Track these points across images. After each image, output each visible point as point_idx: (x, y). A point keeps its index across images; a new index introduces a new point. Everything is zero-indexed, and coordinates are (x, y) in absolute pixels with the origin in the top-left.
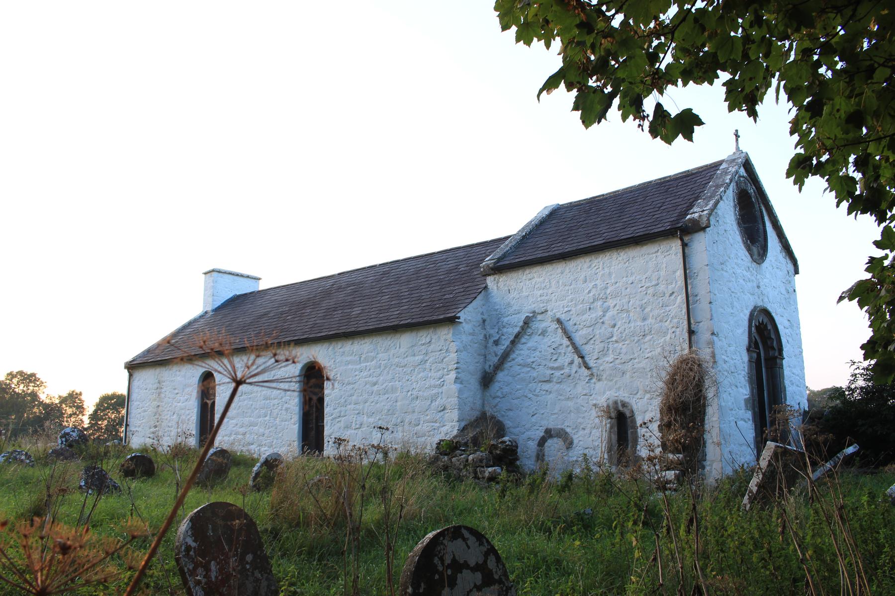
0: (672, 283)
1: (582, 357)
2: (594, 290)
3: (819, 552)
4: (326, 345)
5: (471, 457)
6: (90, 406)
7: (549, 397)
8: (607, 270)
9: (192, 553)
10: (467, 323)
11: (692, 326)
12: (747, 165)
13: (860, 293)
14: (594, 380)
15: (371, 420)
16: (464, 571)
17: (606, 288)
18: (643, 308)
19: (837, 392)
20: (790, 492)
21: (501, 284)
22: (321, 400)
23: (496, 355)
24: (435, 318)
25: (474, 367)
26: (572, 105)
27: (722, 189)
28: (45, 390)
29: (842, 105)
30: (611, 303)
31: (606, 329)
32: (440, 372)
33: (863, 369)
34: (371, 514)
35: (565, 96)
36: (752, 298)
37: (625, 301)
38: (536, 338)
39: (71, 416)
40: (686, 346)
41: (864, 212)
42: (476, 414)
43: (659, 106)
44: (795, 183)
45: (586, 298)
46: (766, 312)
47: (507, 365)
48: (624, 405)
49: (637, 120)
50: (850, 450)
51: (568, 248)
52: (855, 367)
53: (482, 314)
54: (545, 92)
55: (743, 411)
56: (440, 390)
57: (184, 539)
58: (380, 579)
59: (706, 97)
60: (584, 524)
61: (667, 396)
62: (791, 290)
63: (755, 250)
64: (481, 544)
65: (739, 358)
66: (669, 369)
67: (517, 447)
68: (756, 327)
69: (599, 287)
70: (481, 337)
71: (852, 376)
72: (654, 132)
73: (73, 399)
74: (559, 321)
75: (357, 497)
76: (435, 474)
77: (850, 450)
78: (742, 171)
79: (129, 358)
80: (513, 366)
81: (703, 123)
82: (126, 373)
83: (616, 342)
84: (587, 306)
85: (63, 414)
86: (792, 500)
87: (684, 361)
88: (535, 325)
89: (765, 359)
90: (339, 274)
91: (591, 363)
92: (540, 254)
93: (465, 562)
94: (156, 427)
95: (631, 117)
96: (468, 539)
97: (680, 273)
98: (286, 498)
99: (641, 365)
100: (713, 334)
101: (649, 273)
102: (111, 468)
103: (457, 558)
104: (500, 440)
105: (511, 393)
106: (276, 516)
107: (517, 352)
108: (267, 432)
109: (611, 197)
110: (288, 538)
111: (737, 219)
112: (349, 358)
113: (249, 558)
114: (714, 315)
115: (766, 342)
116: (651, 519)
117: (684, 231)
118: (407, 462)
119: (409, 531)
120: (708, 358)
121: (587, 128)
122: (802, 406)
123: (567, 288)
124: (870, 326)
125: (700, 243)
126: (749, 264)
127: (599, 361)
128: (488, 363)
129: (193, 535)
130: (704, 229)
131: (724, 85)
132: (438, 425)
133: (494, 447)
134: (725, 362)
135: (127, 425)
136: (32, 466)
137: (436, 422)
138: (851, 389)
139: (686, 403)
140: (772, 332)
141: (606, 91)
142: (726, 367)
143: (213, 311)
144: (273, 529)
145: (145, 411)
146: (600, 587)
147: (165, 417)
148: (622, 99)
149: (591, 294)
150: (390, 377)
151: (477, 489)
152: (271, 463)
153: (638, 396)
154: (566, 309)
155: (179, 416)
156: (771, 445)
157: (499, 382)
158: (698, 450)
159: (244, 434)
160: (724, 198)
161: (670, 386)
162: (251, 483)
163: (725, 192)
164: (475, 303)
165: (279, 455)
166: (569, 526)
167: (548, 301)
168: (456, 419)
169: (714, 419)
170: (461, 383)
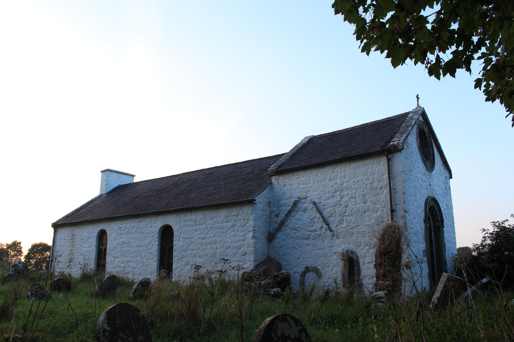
1: (328, 225)
2: (335, 185)
4: (175, 215)
5: (263, 282)
6: (25, 251)
7: (308, 247)
9: (107, 334)
10: (260, 203)
11: (393, 207)
12: (424, 115)
14: (335, 238)
17: (343, 184)
18: (364, 196)
21: (280, 181)
22: (171, 248)
23: (277, 223)
24: (241, 200)
27: (410, 128)
30: (345, 193)
31: (342, 208)
32: (244, 232)
36: (426, 191)
37: (353, 192)
38: (301, 213)
39: (13, 256)
45: (331, 190)
46: (434, 200)
48: (353, 252)
50: (484, 280)
51: (320, 161)
52: (485, 232)
53: (269, 198)
56: (243, 243)
57: (102, 325)
61: (379, 247)
62: (448, 188)
63: (428, 164)
64: (297, 325)
65: (420, 226)
67: (290, 276)
70: (268, 212)
71: (483, 238)
72: (431, 73)
73: (16, 246)
74: (314, 203)
77: (484, 280)
78: (421, 118)
79: (55, 220)
82: (52, 230)
83: (348, 216)
87: (389, 227)
88: (300, 205)
89: (434, 228)
90: (183, 174)
91: (333, 228)
92: (303, 164)
97: (386, 176)
99: (362, 230)
100: (405, 212)
101: (368, 176)
104: (280, 273)
105: (285, 245)
108: (138, 266)
109: (344, 132)
111: (418, 146)
112: (188, 223)
115: (435, 217)
118: (224, 286)
123: (319, 184)
125: (398, 159)
126: (425, 172)
127: (338, 227)
129: (108, 323)
130: (400, 151)
131: (452, 53)
132: (241, 263)
133: (277, 276)
134: (412, 228)
137: (240, 262)
138: (483, 246)
139: (390, 249)
143: (106, 194)
147: (77, 256)
149: (334, 188)
150: (213, 234)
152: (145, 284)
153: (361, 247)
154: (318, 196)
155: (84, 256)
157: (278, 239)
160: (411, 133)
162: (131, 295)
165: (149, 279)
168: (253, 260)
170: (256, 239)
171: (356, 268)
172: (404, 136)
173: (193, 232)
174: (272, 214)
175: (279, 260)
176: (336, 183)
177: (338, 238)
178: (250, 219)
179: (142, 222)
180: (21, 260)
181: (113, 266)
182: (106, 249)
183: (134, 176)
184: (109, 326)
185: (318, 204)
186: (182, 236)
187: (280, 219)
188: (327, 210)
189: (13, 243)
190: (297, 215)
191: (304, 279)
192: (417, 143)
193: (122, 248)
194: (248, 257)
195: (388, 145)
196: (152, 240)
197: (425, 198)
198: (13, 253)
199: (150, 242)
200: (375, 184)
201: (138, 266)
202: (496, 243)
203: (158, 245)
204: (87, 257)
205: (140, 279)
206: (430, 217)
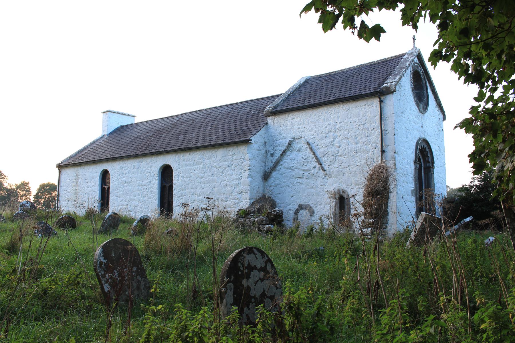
0: (373, 123)
1: (321, 164)
3: (443, 267)
5: (256, 219)
6: (34, 191)
8: (336, 115)
9: (103, 265)
10: (255, 143)
13: (467, 125)
14: (327, 177)
15: (200, 198)
16: (254, 270)
17: (336, 125)
18: (356, 137)
19: (464, 189)
20: (432, 240)
21: (276, 122)
22: (171, 187)
23: (272, 162)
24: (237, 140)
25: (259, 169)
26: (318, 20)
27: (404, 70)
28: (7, 181)
29: (459, 25)
30: (338, 133)
34: (202, 247)
35: (314, 15)
36: (418, 133)
37: (346, 132)
38: (295, 153)
39: (23, 196)
40: (380, 159)
41: (473, 83)
42: (260, 195)
43: (363, 22)
44: (432, 65)
46: (426, 141)
47: (278, 168)
48: (344, 192)
49: (351, 29)
50: (468, 219)
53: (265, 138)
55: (410, 197)
56: (240, 182)
57: (99, 258)
58: (206, 281)
59: (388, 18)
60: (320, 255)
61: (368, 187)
64: (263, 257)
66: (370, 172)
67: (283, 214)
68: (420, 150)
69: (332, 124)
70: (264, 152)
72: (360, 36)
73: (24, 186)
74: (308, 143)
75: (193, 239)
76: (237, 227)
77: (468, 219)
78: (416, 60)
81: (385, 32)
82: (57, 170)
84: (324, 135)
85: (18, 195)
86: (433, 243)
87: (378, 167)
88: (294, 145)
89: (424, 168)
91: (326, 168)
92: (299, 105)
93: (255, 266)
94: (75, 201)
95: (348, 27)
96: (257, 254)
97: (378, 117)
98: (153, 238)
99: (354, 169)
100: (395, 152)
103: (251, 264)
106: (148, 248)
107: (284, 161)
109: (340, 73)
110: (154, 260)
112: (187, 163)
113: (134, 269)
115: (425, 158)
116: (356, 251)
118: (218, 223)
119: (222, 257)
120: (392, 166)
121: (325, 32)
122: (443, 195)
123: (313, 124)
124: (474, 145)
125: (390, 100)
126: (418, 114)
127: (331, 167)
128: (267, 167)
129: (104, 256)
130: (392, 93)
131: (401, 11)
132: (238, 201)
133: (270, 214)
134: (401, 169)
136: (5, 222)
137: (237, 199)
139: (379, 190)
141: (336, 13)
142: (401, 171)
143: (108, 135)
144: (146, 255)
145: (68, 192)
146: (326, 286)
147: (79, 195)
148: (344, 17)
150: (211, 173)
151: (260, 236)
152: (144, 221)
153: (352, 187)
154: (312, 137)
155: (89, 195)
158: (384, 218)
160: (405, 75)
161: (370, 181)
163: (406, 71)
165: (148, 216)
166: (310, 256)
167: (302, 132)
169: (394, 200)
170: (252, 178)
173: (192, 171)
175: (274, 198)
176: (330, 124)
179: (142, 162)
180: (30, 199)
181: (115, 206)
182: (109, 188)
185: (312, 145)
188: (320, 150)
189: (22, 183)
190: (291, 155)
192: (411, 85)
193: (124, 187)
194: (244, 196)
195: (381, 87)
196: (153, 180)
197: (416, 140)
198: (22, 193)
199: (150, 182)
200: (367, 126)
201: (140, 204)
204: (90, 196)
205: (140, 217)
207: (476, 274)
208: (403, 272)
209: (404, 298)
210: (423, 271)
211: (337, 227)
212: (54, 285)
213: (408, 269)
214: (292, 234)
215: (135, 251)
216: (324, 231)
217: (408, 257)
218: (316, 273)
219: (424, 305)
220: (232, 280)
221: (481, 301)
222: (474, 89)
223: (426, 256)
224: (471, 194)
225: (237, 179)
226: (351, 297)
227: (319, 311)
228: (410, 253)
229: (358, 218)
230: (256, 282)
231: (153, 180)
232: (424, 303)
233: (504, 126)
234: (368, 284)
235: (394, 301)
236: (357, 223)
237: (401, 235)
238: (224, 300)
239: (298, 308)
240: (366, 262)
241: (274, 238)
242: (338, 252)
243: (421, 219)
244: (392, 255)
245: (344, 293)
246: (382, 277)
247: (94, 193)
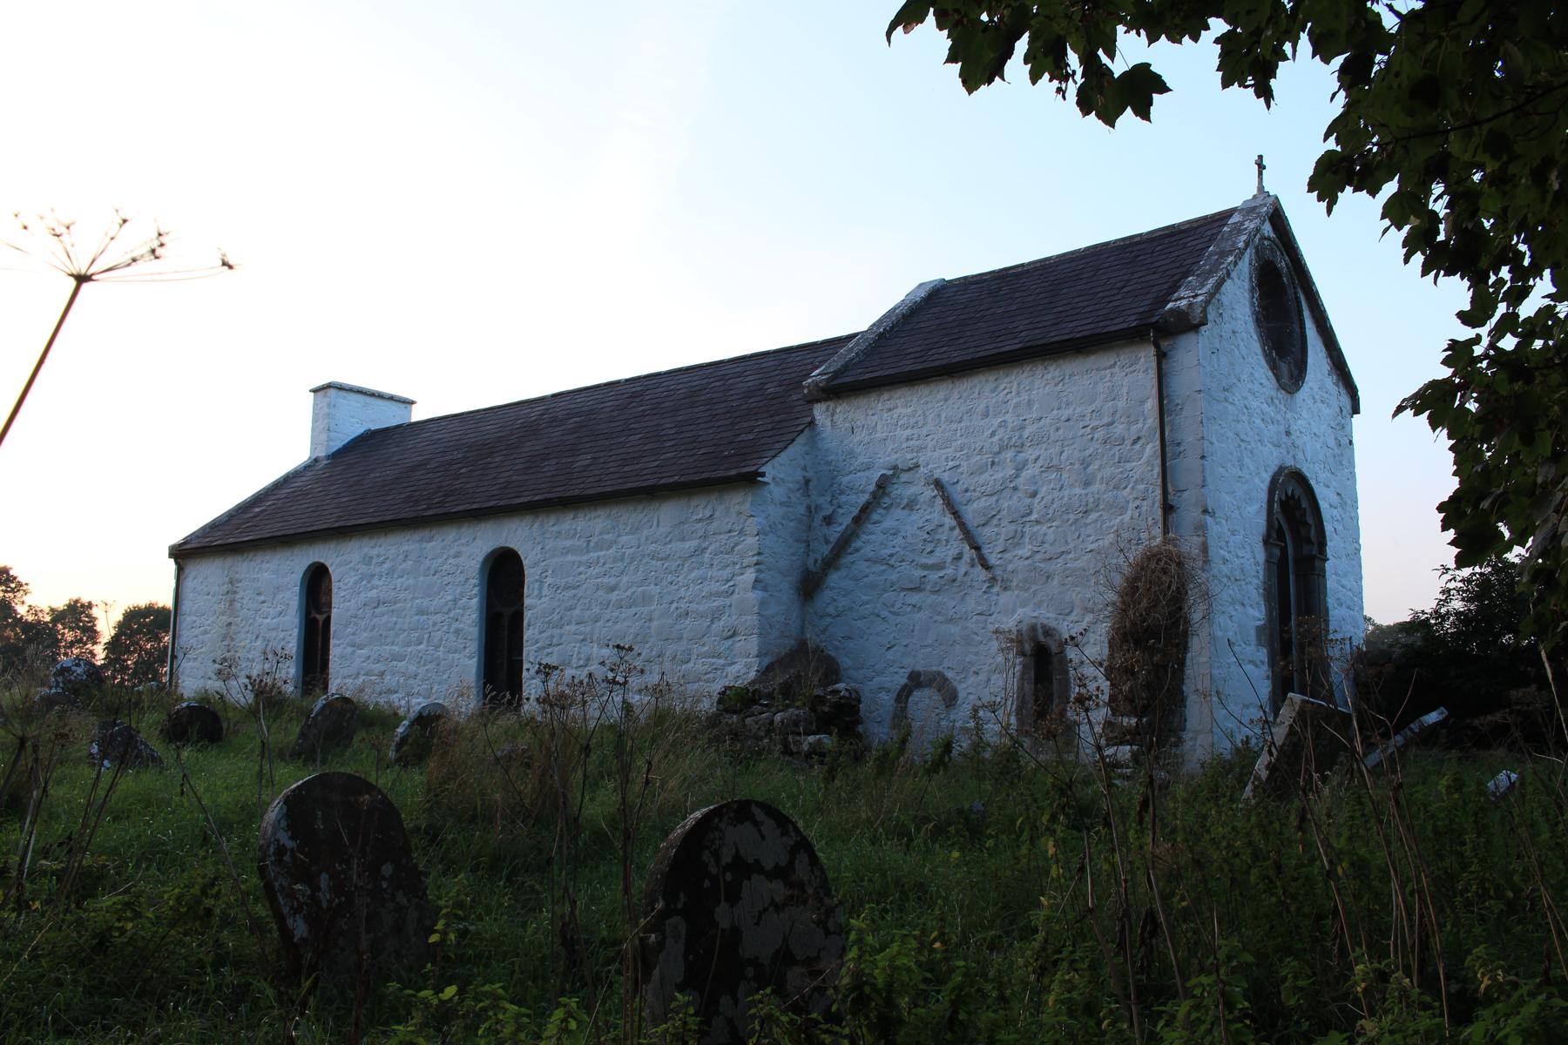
0: (1136, 422)
1: (978, 548)
3: (1360, 868)
4: (528, 519)
5: (778, 717)
6: (106, 627)
8: (1024, 397)
9: (287, 858)
10: (777, 484)
13: (1432, 402)
14: (996, 589)
16: (755, 877)
17: (1023, 428)
18: (1085, 464)
19: (1417, 625)
20: (1324, 779)
21: (839, 418)
22: (519, 616)
23: (827, 542)
24: (721, 474)
27: (1231, 258)
30: (1030, 453)
31: (1020, 499)
32: (729, 570)
33: (1463, 581)
34: (599, 806)
35: (931, 38)
37: (1055, 450)
38: (898, 513)
39: (72, 645)
40: (1158, 531)
45: (987, 445)
46: (1299, 478)
48: (1048, 632)
50: (1432, 717)
51: (956, 356)
53: (805, 469)
54: (900, 29)
55: (1253, 648)
56: (728, 601)
57: (274, 833)
60: (971, 828)
62: (1344, 441)
63: (1284, 368)
64: (785, 833)
65: (1249, 555)
66: (1127, 570)
67: (859, 700)
68: (1283, 504)
69: (1010, 425)
70: (802, 509)
71: (1443, 592)
73: (77, 614)
74: (938, 484)
76: (718, 740)
77: (1432, 717)
78: (1267, 229)
79: (178, 537)
80: (858, 561)
82: (171, 565)
83: (1038, 522)
84: (987, 458)
86: (1326, 792)
87: (1152, 556)
89: (1296, 561)
90: (554, 396)
91: (993, 559)
92: (909, 366)
93: (757, 861)
95: (1046, 76)
97: (1151, 404)
99: (1079, 564)
100: (1205, 511)
101: (1097, 404)
102: (148, 726)
104: (830, 689)
105: (851, 609)
107: (864, 537)
108: (422, 670)
109: (1036, 269)
112: (568, 543)
113: (387, 869)
114: (1209, 480)
115: (1300, 529)
116: (1081, 816)
117: (1162, 330)
121: (970, 93)
123: (954, 426)
124: (1455, 474)
125: (1191, 354)
126: (1273, 393)
127: (1008, 556)
130: (1195, 328)
131: (1217, 41)
132: (722, 661)
133: (820, 700)
134: (1225, 561)
135: (174, 657)
137: (719, 656)
139: (1156, 616)
140: (1308, 512)
142: (1226, 569)
143: (328, 457)
145: (206, 632)
147: (243, 639)
149: (996, 438)
150: (640, 576)
152: (428, 721)
153: (1073, 617)
154: (951, 464)
156: (1296, 697)
159: (382, 674)
160: (1233, 275)
161: (1128, 599)
162: (392, 754)
163: (1236, 264)
164: (791, 450)
166: (940, 831)
167: (921, 449)
168: (755, 651)
170: (765, 589)
171: (1057, 677)
172: (1211, 282)
174: (813, 518)
175: (833, 654)
176: (1003, 424)
177: (1006, 589)
178: (748, 530)
179: (431, 539)
180: (94, 655)
182: (328, 621)
183: (413, 403)
184: (292, 838)
185: (951, 489)
186: (549, 580)
187: (836, 531)
188: (975, 505)
189: (69, 606)
190: (887, 520)
191: (904, 709)
192: (1252, 304)
193: (374, 616)
195: (1161, 311)
196: (462, 595)
197: (1271, 473)
199: (455, 601)
200: (1119, 429)
202: (1479, 610)
203: (481, 609)
206: (1285, 526)
207: (1466, 890)
208: (1233, 880)
209: (1233, 971)
210: (1295, 880)
211: (1027, 743)
212: (131, 920)
213: (1248, 873)
214: (886, 764)
215: (387, 811)
216: (987, 755)
217: (1248, 834)
218: (958, 884)
219: (1302, 989)
220: (680, 905)
221: (1494, 978)
222: (1457, 291)
223: (1304, 832)
224: (1441, 641)
225: (719, 594)
226: (1065, 965)
227: (955, 1012)
228: (1253, 819)
229: (1087, 710)
230: (760, 914)
231: (462, 595)
232: (1300, 983)
233: (1556, 408)
234: (1121, 920)
235: (1204, 979)
236: (1085, 728)
237: (1225, 767)
238: (656, 972)
239: (889, 1003)
240: (1113, 850)
241: (831, 776)
242: (1028, 817)
243: (1287, 714)
244: (1196, 827)
245: (1044, 949)
246: (1166, 898)
247: (282, 635)
